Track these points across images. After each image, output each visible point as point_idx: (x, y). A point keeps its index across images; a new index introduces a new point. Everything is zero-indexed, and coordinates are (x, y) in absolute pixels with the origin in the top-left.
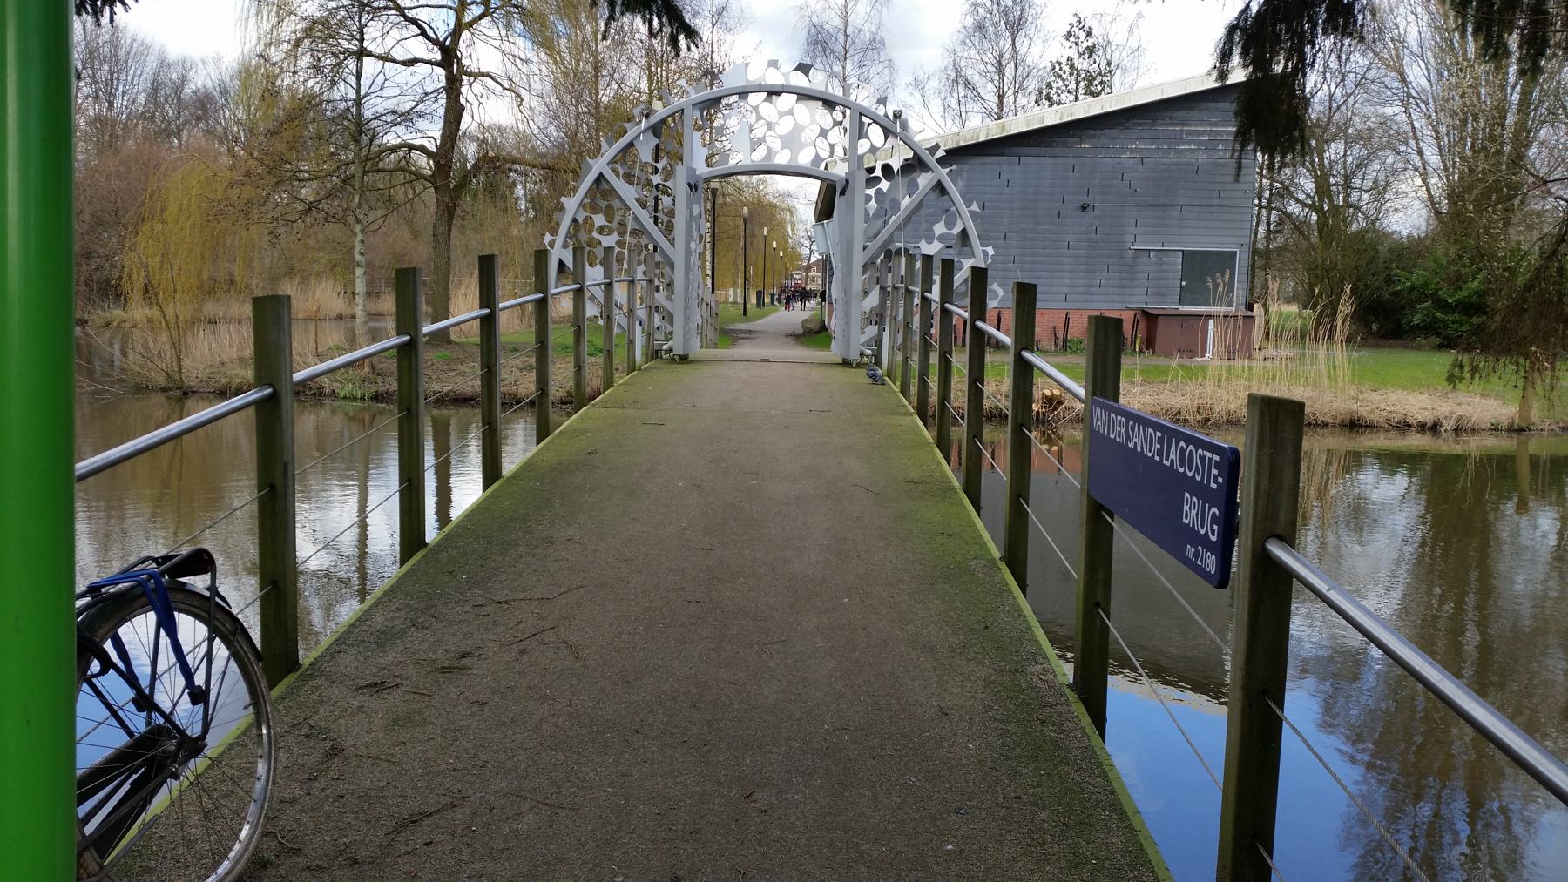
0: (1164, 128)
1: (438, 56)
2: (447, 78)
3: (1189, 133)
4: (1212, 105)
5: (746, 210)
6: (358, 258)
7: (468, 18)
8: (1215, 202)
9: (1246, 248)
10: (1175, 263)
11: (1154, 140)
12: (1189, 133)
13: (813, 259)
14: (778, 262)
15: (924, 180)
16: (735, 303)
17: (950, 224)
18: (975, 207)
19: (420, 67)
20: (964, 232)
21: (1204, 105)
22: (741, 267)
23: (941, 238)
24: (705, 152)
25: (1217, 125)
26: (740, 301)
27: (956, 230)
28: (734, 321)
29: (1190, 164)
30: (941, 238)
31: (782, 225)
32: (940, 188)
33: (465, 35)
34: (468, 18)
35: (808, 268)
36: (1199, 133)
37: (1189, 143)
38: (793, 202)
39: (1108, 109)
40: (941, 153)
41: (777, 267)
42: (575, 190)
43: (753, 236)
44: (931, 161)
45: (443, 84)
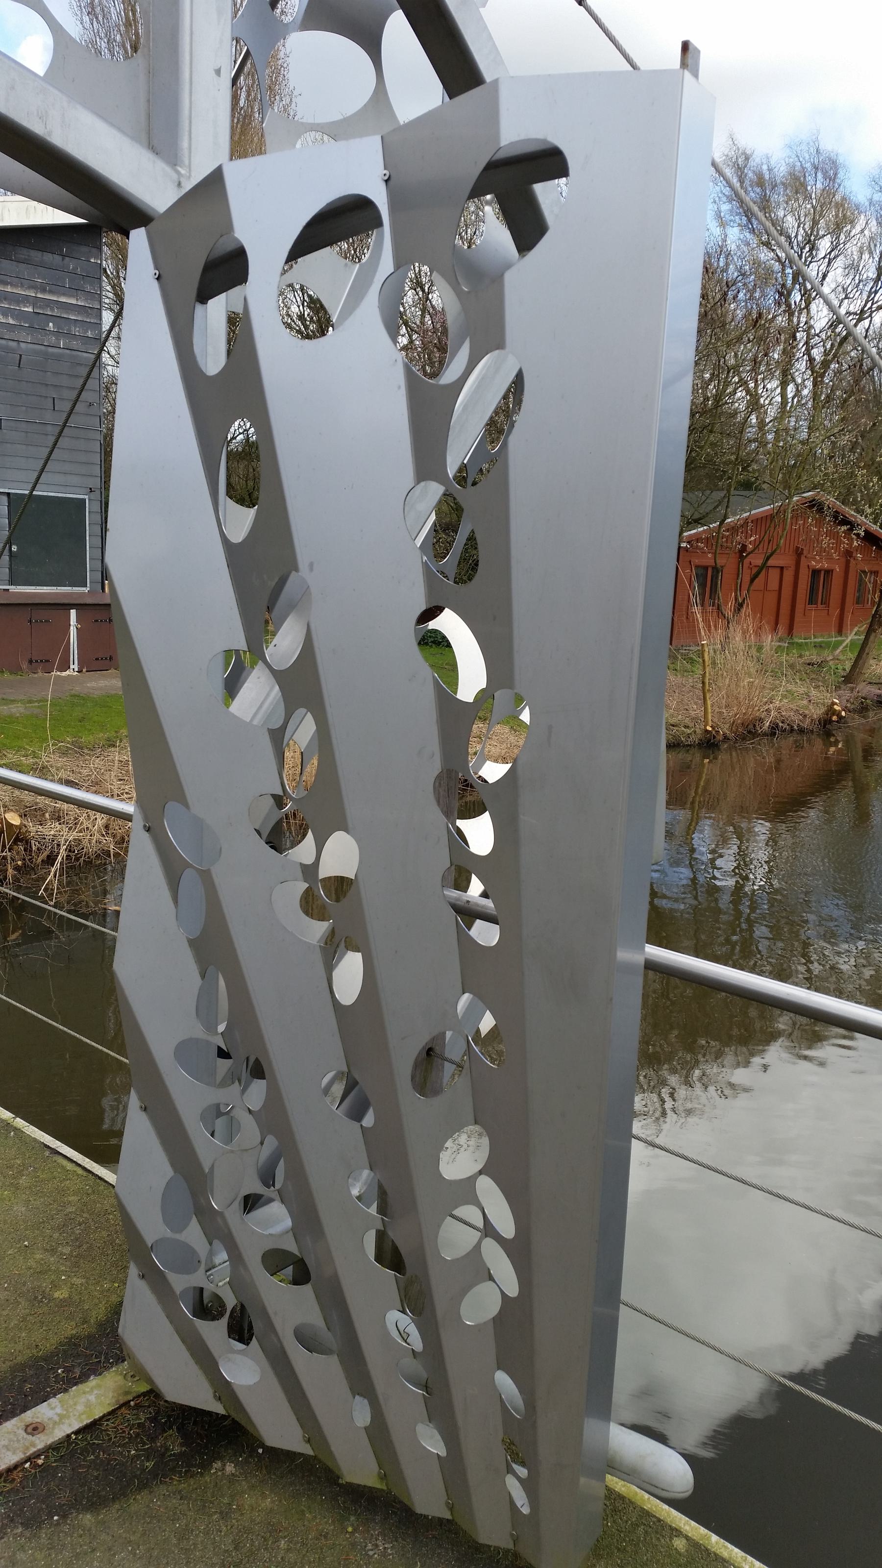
21: (24, 253)
25: (44, 291)
36: (26, 300)
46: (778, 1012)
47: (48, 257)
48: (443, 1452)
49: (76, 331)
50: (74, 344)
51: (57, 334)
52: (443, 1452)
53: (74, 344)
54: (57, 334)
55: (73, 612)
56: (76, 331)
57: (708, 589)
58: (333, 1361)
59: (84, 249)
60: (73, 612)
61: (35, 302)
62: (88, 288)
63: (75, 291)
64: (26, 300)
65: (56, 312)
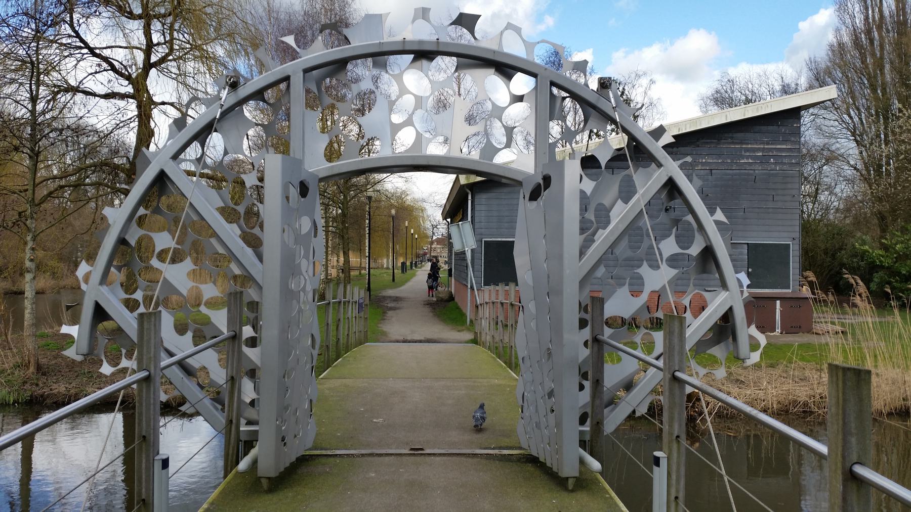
0: (726, 146)
1: (130, 89)
2: (139, 107)
3: (747, 150)
4: (764, 128)
5: (393, 212)
6: (28, 264)
7: (154, 59)
8: (771, 205)
9: (797, 241)
10: (741, 254)
11: (719, 156)
12: (747, 150)
13: (434, 238)
14: (414, 241)
15: (648, 184)
16: (388, 268)
17: (684, 241)
18: (720, 215)
19: (102, 90)
20: (708, 253)
21: (758, 128)
22: (391, 245)
23: (673, 261)
24: (322, 142)
25: (768, 144)
26: (391, 267)
27: (695, 250)
28: (386, 287)
29: (748, 174)
30: (673, 261)
31: (416, 218)
32: (671, 187)
33: (153, 71)
34: (154, 59)
35: (432, 243)
36: (758, 150)
37: (747, 157)
38: (425, 205)
39: (684, 131)
40: (667, 139)
41: (414, 245)
42: (126, 193)
43: (398, 230)
44: (656, 147)
45: (136, 113)
46: (183, 154)
47: (771, 128)
48: (303, 233)
49: (786, 161)
50: (785, 167)
51: (775, 164)
52: (303, 233)
53: (785, 167)
54: (775, 164)
55: (778, 302)
56: (786, 161)
57: (674, 482)
58: (111, 72)
59: (791, 120)
60: (778, 302)
61: (763, 150)
62: (793, 139)
63: (785, 141)
64: (758, 150)
65: (775, 153)
